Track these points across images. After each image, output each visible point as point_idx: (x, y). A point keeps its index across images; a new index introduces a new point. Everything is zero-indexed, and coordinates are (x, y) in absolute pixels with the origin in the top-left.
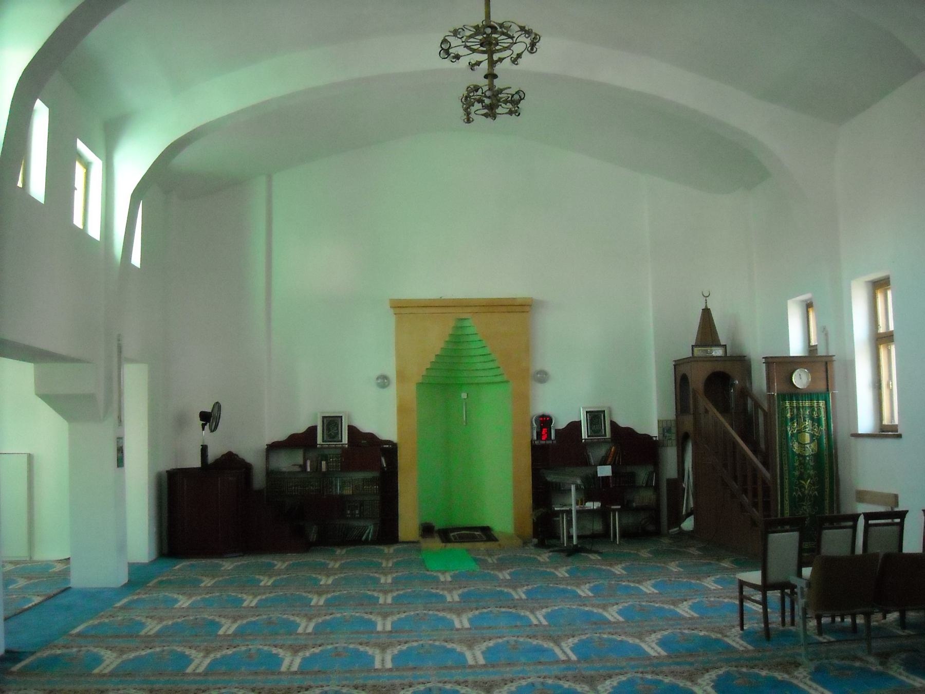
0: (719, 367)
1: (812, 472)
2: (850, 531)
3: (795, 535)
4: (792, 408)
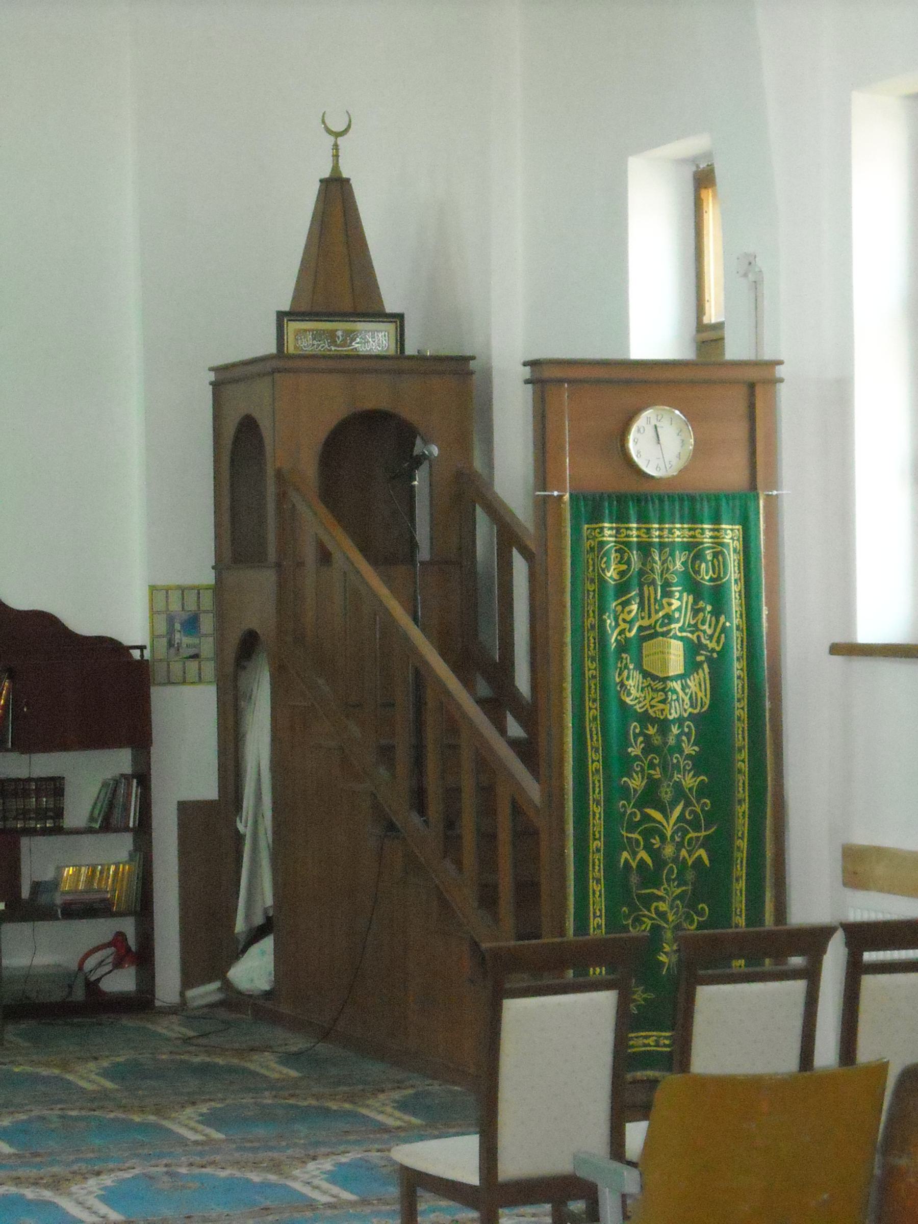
0: (375, 396)
1: (689, 781)
2: (799, 986)
3: (604, 1001)
4: (623, 547)
